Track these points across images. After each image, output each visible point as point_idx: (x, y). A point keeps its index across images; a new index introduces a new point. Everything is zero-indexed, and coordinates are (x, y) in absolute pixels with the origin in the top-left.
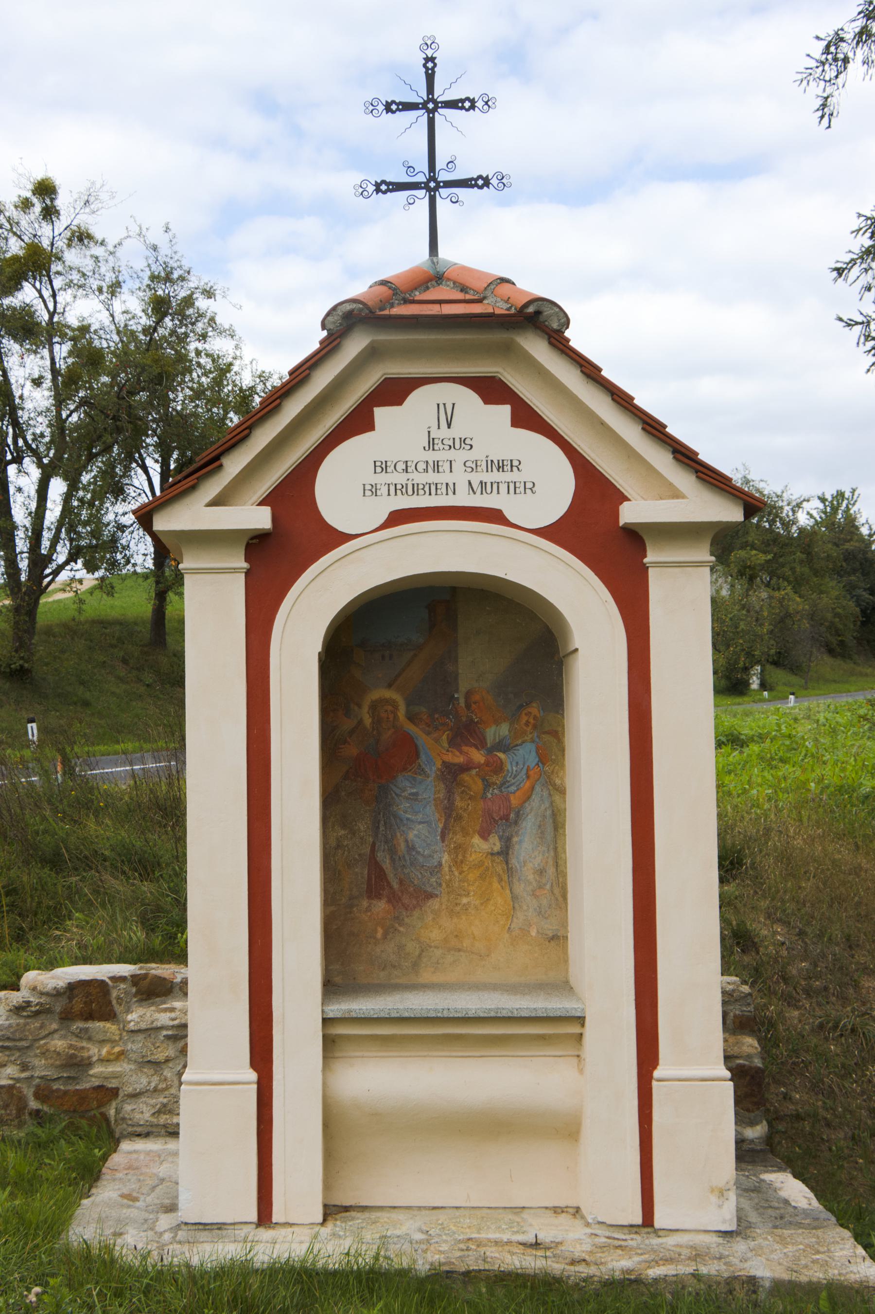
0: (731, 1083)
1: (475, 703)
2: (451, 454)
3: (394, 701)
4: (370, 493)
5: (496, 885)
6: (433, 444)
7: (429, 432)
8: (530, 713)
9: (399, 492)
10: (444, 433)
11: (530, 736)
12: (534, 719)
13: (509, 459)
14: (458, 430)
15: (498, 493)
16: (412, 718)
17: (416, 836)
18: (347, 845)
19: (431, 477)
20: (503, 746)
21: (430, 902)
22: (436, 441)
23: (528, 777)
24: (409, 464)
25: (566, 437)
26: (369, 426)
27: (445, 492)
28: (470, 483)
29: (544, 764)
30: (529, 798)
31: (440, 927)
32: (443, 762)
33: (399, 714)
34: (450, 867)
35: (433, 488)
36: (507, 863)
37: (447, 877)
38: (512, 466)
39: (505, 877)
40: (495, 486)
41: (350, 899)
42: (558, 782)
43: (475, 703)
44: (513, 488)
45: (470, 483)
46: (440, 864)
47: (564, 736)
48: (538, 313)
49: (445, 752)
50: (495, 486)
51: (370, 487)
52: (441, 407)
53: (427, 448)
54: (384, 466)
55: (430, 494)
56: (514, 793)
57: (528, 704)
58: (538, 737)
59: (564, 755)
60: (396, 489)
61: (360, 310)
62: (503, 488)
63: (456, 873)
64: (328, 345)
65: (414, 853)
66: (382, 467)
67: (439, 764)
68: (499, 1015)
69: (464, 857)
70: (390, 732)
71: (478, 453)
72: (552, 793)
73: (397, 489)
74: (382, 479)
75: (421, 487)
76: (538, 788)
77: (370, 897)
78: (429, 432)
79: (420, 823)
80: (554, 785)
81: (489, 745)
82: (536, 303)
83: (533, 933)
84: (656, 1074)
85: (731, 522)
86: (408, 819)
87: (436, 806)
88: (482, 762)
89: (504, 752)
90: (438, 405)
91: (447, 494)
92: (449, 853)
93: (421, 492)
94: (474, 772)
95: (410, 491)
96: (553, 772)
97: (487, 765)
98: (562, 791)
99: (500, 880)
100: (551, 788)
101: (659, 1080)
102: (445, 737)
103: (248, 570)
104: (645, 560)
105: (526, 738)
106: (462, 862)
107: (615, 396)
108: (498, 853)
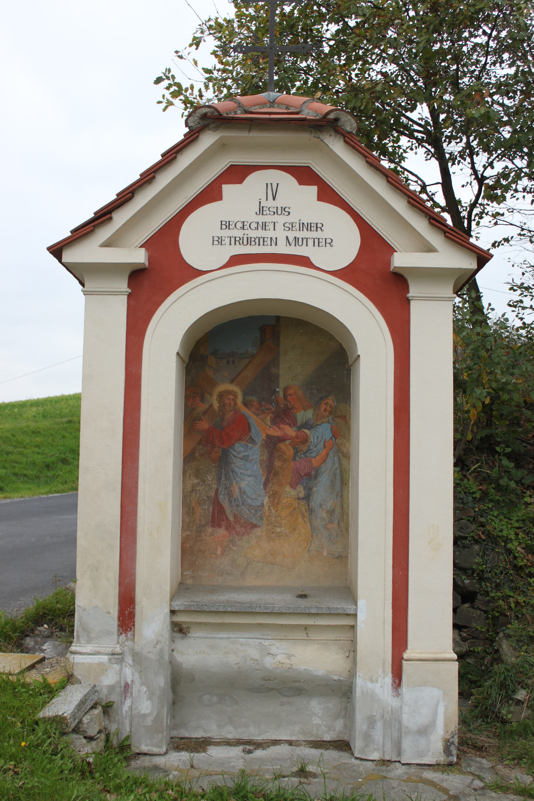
0: (457, 663)
1: (290, 395)
2: (275, 218)
3: (235, 392)
4: (217, 243)
5: (300, 520)
6: (263, 211)
7: (260, 202)
8: (328, 403)
9: (237, 243)
10: (270, 203)
11: (327, 419)
12: (330, 408)
13: (315, 222)
14: (280, 202)
15: (307, 245)
16: (246, 404)
17: (246, 485)
18: (199, 490)
19: (260, 233)
20: (307, 425)
21: (255, 530)
22: (265, 209)
23: (325, 447)
24: (245, 223)
25: (355, 209)
26: (218, 197)
27: (269, 244)
28: (287, 238)
29: (336, 438)
30: (325, 461)
31: (261, 548)
32: (267, 435)
33: (237, 401)
34: (269, 507)
35: (261, 240)
36: (308, 505)
37: (267, 514)
38: (317, 227)
39: (307, 515)
40: (305, 241)
41: (200, 527)
42: (345, 450)
43: (290, 395)
44: (317, 242)
45: (287, 238)
46: (262, 505)
47: (350, 420)
48: (337, 120)
49: (268, 428)
50: (305, 241)
51: (217, 239)
52: (269, 186)
53: (258, 213)
54: (227, 224)
55: (259, 245)
56: (315, 457)
57: (326, 397)
58: (333, 420)
59: (349, 432)
60: (235, 241)
61: (212, 113)
62: (310, 242)
63: (273, 511)
64: (189, 138)
65: (245, 497)
66: (226, 225)
67: (264, 436)
68: (296, 612)
69: (279, 500)
70: (231, 414)
71: (293, 218)
72: (341, 458)
73: (237, 241)
74: (226, 233)
75: (253, 239)
76: (331, 454)
77: (213, 526)
78: (260, 202)
79: (250, 476)
80: (343, 453)
81: (298, 424)
82: (335, 112)
83: (325, 554)
84: (405, 656)
85: (469, 269)
86: (241, 473)
87: (261, 464)
88: (294, 435)
89: (309, 429)
90: (267, 184)
91: (271, 245)
92: (269, 497)
93: (253, 243)
94: (288, 442)
95: (245, 243)
96: (342, 443)
97: (297, 438)
98: (347, 456)
99: (303, 516)
100: (340, 454)
101: (406, 660)
102: (268, 418)
103: (130, 293)
104: (409, 295)
105: (324, 420)
106: (277, 504)
107: (389, 179)
108: (303, 498)
